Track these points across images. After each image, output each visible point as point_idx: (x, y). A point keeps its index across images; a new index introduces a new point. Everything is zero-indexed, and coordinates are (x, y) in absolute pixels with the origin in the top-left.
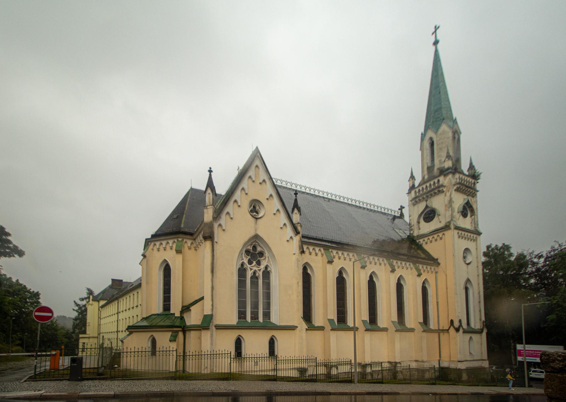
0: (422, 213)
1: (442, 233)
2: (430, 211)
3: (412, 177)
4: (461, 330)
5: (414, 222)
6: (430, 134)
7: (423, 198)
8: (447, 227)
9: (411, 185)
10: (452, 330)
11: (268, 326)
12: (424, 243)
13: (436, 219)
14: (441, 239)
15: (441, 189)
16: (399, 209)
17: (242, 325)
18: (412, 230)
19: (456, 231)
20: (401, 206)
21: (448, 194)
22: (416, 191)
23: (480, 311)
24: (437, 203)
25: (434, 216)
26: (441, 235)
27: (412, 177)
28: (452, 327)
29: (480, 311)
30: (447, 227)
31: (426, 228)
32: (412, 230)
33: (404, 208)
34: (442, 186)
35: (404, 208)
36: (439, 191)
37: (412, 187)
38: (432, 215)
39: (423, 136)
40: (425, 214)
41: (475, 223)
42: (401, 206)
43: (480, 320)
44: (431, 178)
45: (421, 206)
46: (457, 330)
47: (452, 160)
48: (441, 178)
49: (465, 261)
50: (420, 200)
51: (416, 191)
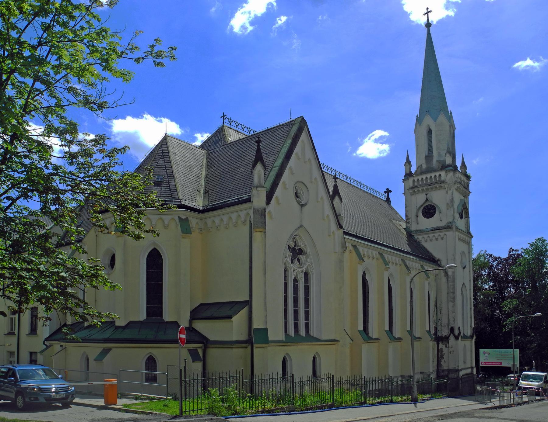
0: (421, 206)
1: (443, 233)
2: (430, 205)
3: (408, 162)
4: (460, 338)
5: (412, 215)
6: (428, 121)
7: (423, 190)
8: (448, 227)
9: (408, 172)
10: (452, 338)
11: (310, 339)
12: (423, 240)
13: (437, 215)
14: (442, 239)
15: (443, 185)
16: (385, 192)
17: (288, 339)
18: (409, 223)
19: (457, 233)
20: (388, 189)
21: (450, 192)
22: (414, 180)
23: (471, 317)
24: (438, 198)
25: (435, 212)
26: (442, 234)
27: (408, 162)
28: (452, 335)
29: (471, 317)
30: (448, 227)
31: (426, 223)
32: (409, 223)
33: (391, 191)
34: (444, 182)
35: (391, 191)
36: (441, 187)
37: (409, 175)
38: (431, 211)
39: (419, 120)
40: (424, 208)
41: (467, 225)
42: (388, 189)
43: (471, 326)
44: (430, 170)
45: (420, 199)
46: (457, 338)
47: (20, 4)
48: (443, 173)
49: (299, 203)
50: (419, 191)
51: (414, 180)
